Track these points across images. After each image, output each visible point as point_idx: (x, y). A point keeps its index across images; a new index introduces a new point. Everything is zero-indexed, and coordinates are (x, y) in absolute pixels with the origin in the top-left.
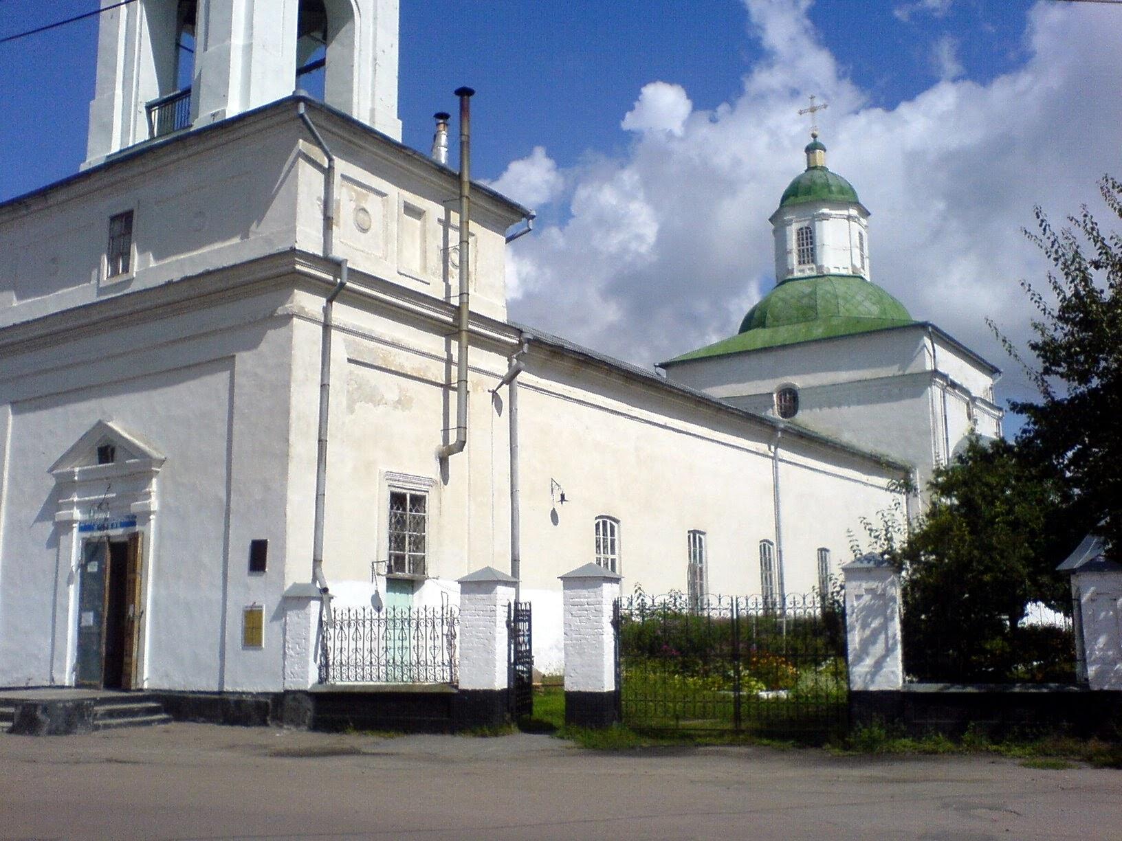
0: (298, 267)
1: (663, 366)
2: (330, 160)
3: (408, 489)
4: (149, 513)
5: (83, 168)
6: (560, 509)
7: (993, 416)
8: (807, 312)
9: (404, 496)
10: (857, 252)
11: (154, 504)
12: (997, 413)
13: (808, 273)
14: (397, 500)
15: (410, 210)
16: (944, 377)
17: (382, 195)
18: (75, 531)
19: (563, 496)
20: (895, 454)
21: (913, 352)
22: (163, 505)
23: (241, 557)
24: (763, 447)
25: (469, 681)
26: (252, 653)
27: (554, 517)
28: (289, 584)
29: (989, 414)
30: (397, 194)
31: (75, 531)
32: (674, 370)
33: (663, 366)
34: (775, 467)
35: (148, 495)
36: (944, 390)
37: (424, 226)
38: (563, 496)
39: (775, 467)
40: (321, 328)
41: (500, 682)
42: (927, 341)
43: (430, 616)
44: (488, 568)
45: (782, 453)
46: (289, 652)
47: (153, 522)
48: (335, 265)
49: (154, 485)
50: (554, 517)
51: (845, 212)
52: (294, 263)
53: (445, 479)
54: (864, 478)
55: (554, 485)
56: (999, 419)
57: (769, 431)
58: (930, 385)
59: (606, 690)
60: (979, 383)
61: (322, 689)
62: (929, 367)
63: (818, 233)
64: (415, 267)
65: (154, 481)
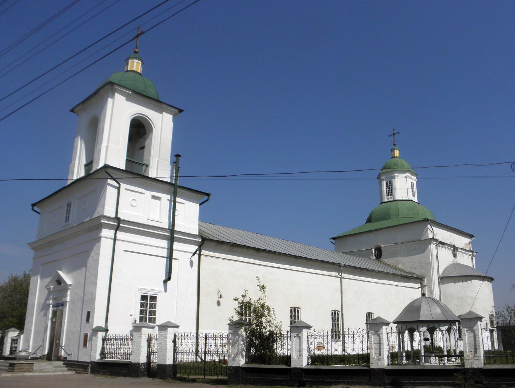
0: (102, 221)
1: (333, 239)
2: (119, 184)
3: (149, 294)
4: (67, 302)
5: (98, 168)
6: (221, 300)
7: (470, 255)
8: (386, 216)
9: (147, 296)
10: (410, 191)
11: (68, 299)
12: (471, 253)
13: (391, 200)
14: (144, 298)
15: (154, 197)
16: (437, 240)
17: (143, 193)
18: (51, 307)
19: (221, 295)
20: (418, 272)
21: (424, 230)
22: (71, 300)
23: (85, 317)
24: (336, 274)
25: (133, 360)
26: (85, 349)
27: (219, 303)
28: (94, 327)
29: (466, 254)
30: (149, 194)
31: (51, 307)
32: (337, 240)
33: (333, 239)
34: (341, 281)
35: (67, 296)
36: (437, 245)
37: (161, 202)
38: (221, 295)
39: (341, 281)
40: (176, 229)
41: (143, 359)
42: (429, 226)
43: (351, 333)
44: (169, 322)
45: (344, 275)
46: (93, 349)
47: (68, 305)
48: (118, 219)
49: (69, 293)
50: (219, 303)
51: (405, 175)
52: (101, 220)
53: (166, 290)
54: (396, 283)
55: (219, 291)
56: (473, 256)
57: (338, 267)
58: (430, 244)
59: (167, 364)
60: (461, 241)
61: (101, 361)
62: (430, 236)
63: (393, 184)
64: (157, 218)
65: (69, 291)
